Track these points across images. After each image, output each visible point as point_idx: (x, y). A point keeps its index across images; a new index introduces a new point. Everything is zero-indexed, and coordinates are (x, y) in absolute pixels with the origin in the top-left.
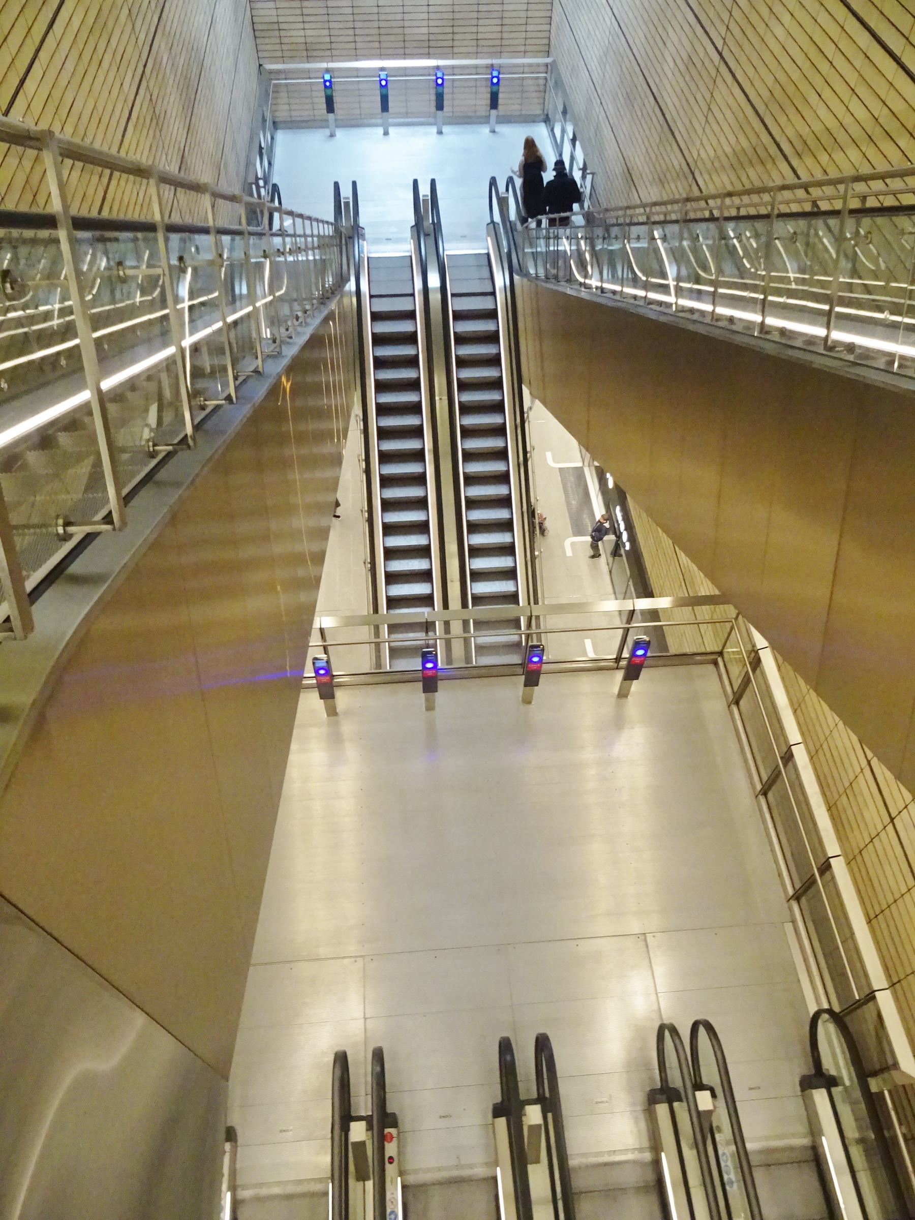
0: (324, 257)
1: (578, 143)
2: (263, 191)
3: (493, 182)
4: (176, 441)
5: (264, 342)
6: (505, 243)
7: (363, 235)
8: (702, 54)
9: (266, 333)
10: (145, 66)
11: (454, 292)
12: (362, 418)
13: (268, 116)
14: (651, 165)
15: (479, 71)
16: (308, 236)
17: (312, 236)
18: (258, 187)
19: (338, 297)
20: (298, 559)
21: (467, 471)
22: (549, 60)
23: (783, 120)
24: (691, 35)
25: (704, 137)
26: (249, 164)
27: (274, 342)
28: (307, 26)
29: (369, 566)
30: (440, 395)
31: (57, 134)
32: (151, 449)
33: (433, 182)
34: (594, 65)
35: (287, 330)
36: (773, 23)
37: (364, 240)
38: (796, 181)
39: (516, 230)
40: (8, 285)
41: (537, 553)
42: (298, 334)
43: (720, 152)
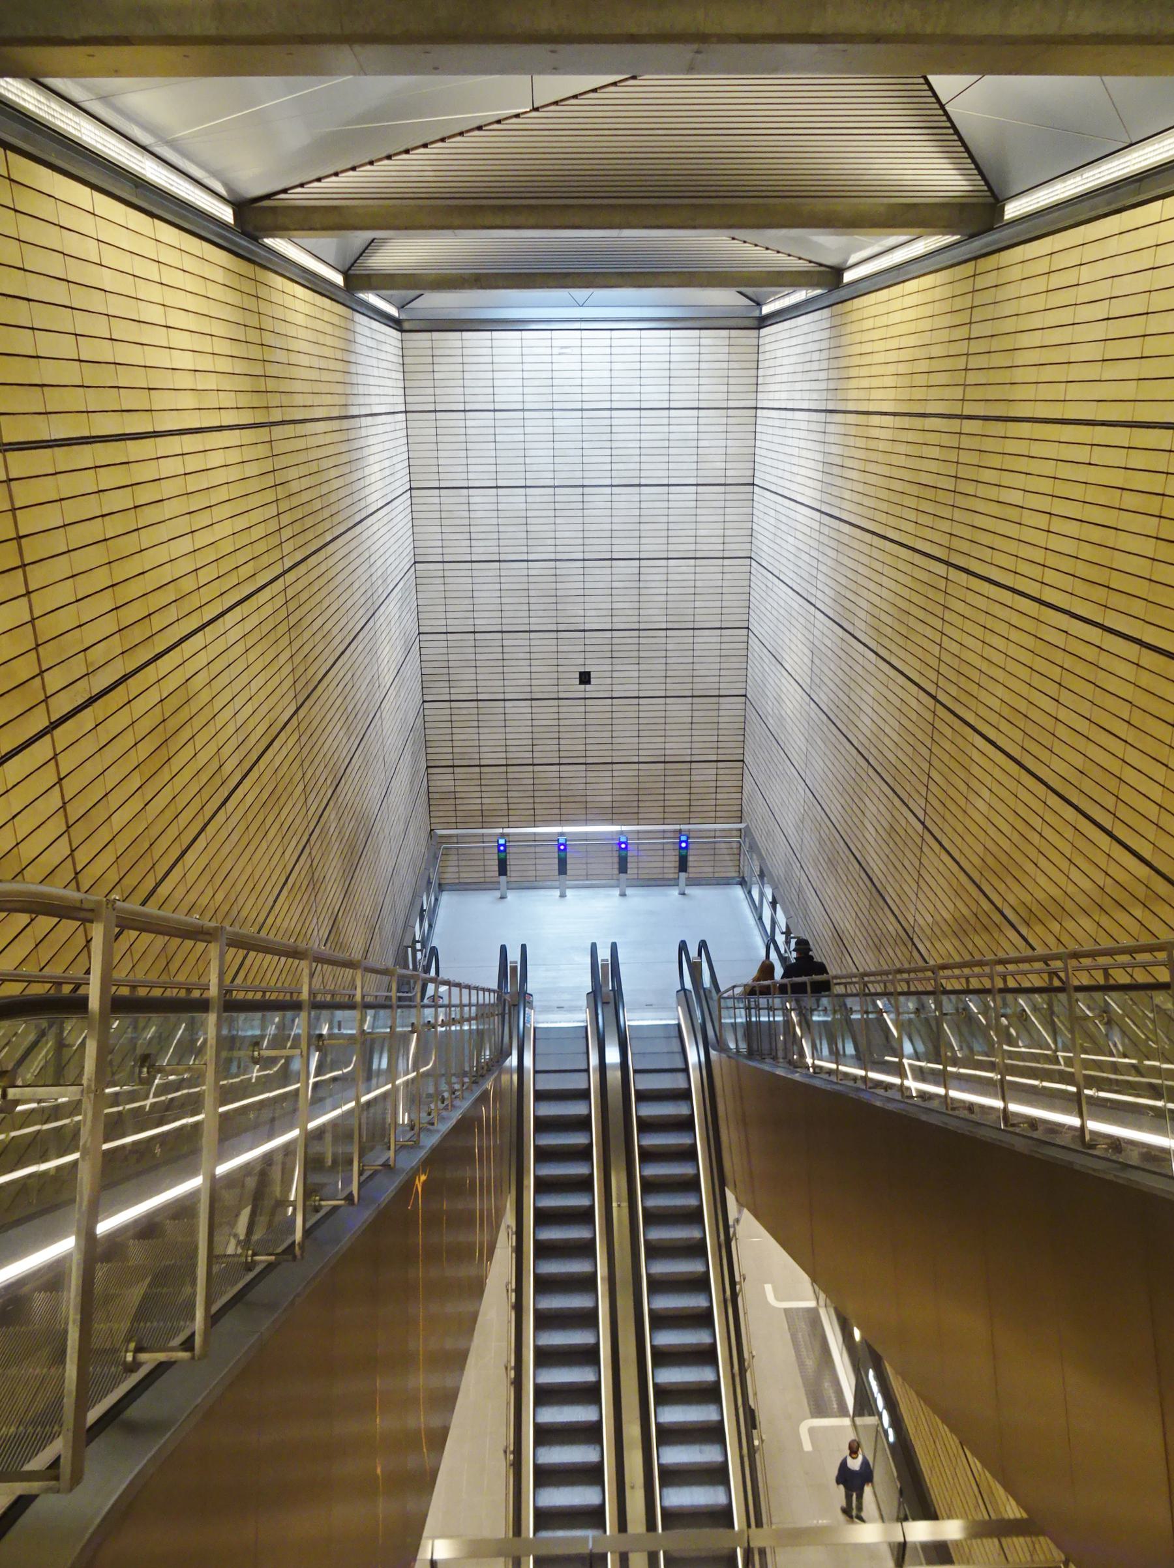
0: (481, 1027)
1: (778, 905)
2: (419, 955)
3: (683, 947)
4: (279, 1250)
5: (399, 1129)
6: (698, 1013)
7: (530, 1003)
8: (903, 822)
9: (403, 1118)
10: (310, 835)
11: (638, 1067)
12: (514, 1229)
13: (434, 880)
14: (863, 929)
15: (667, 835)
16: (465, 1006)
17: (470, 1005)
18: (414, 951)
19: (496, 1074)
20: (409, 1441)
21: (654, 1306)
22: (742, 826)
23: (1001, 887)
24: (890, 806)
25: (919, 902)
26: (407, 926)
27: (412, 1128)
28: (484, 795)
29: (512, 1457)
30: (619, 1200)
31: (228, 928)
32: (249, 1259)
33: (614, 947)
34: (791, 831)
35: (429, 1114)
36: (972, 797)
37: (531, 1008)
38: (1029, 952)
39: (712, 999)
40: (145, 1070)
41: (756, 1443)
42: (442, 1119)
43: (938, 918)
